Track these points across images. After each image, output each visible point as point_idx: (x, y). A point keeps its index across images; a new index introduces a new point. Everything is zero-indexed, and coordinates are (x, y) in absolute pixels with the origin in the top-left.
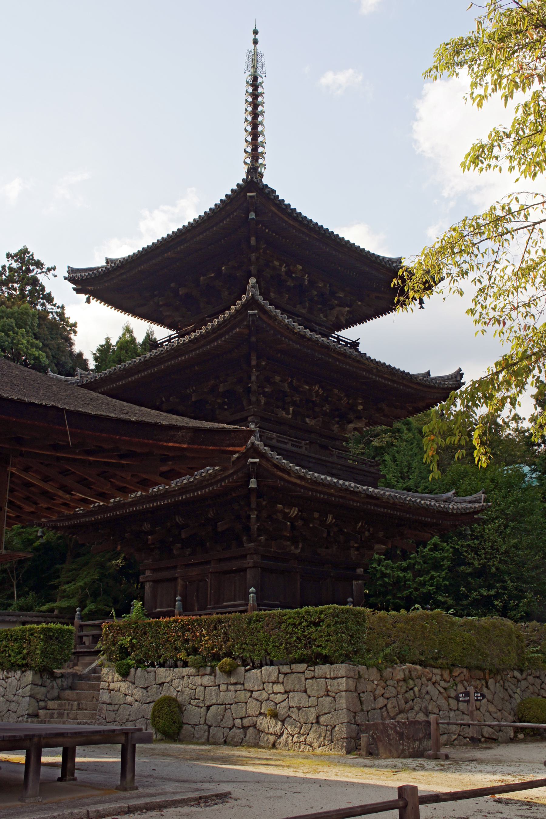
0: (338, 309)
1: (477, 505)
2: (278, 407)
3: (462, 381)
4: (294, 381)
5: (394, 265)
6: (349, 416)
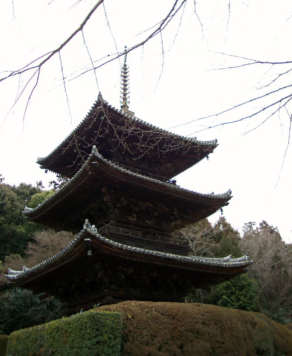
1: (242, 262)
3: (231, 195)
4: (134, 200)
5: (193, 140)
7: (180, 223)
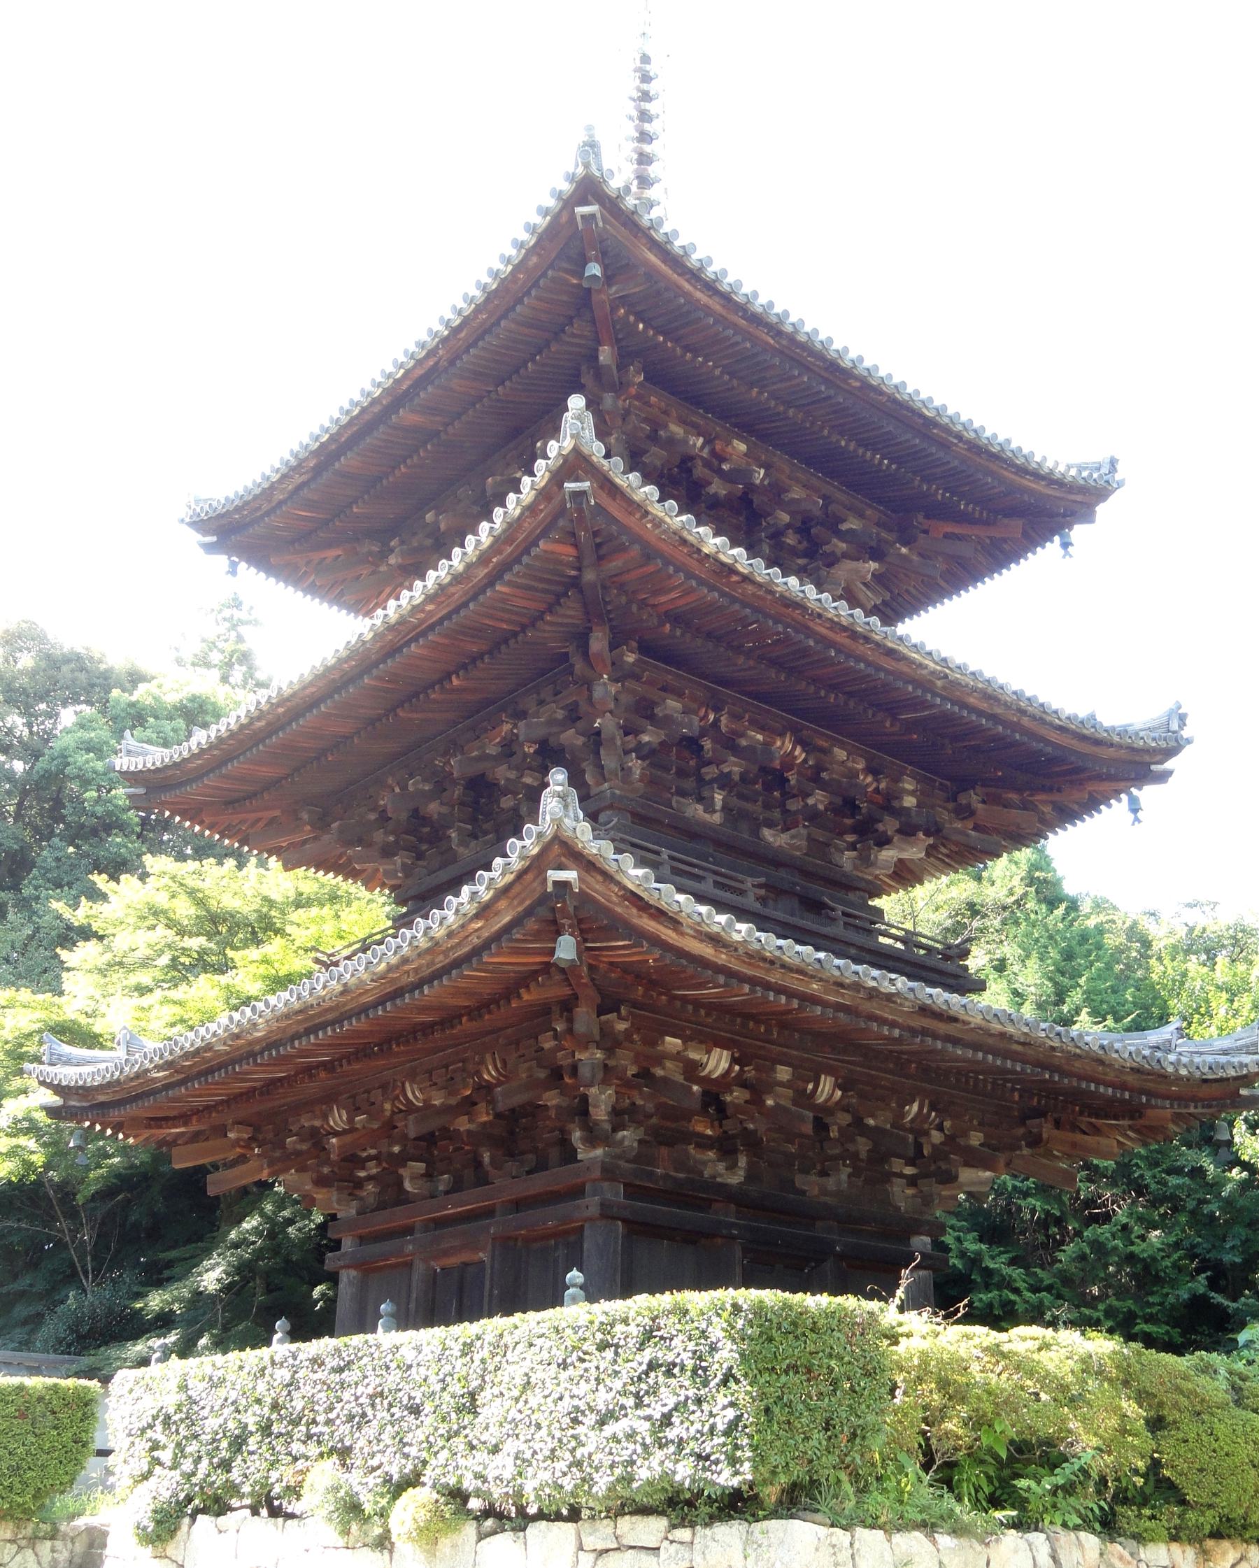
0: (848, 565)
2: (682, 793)
3: (1185, 733)
6: (880, 827)
7: (922, 855)
